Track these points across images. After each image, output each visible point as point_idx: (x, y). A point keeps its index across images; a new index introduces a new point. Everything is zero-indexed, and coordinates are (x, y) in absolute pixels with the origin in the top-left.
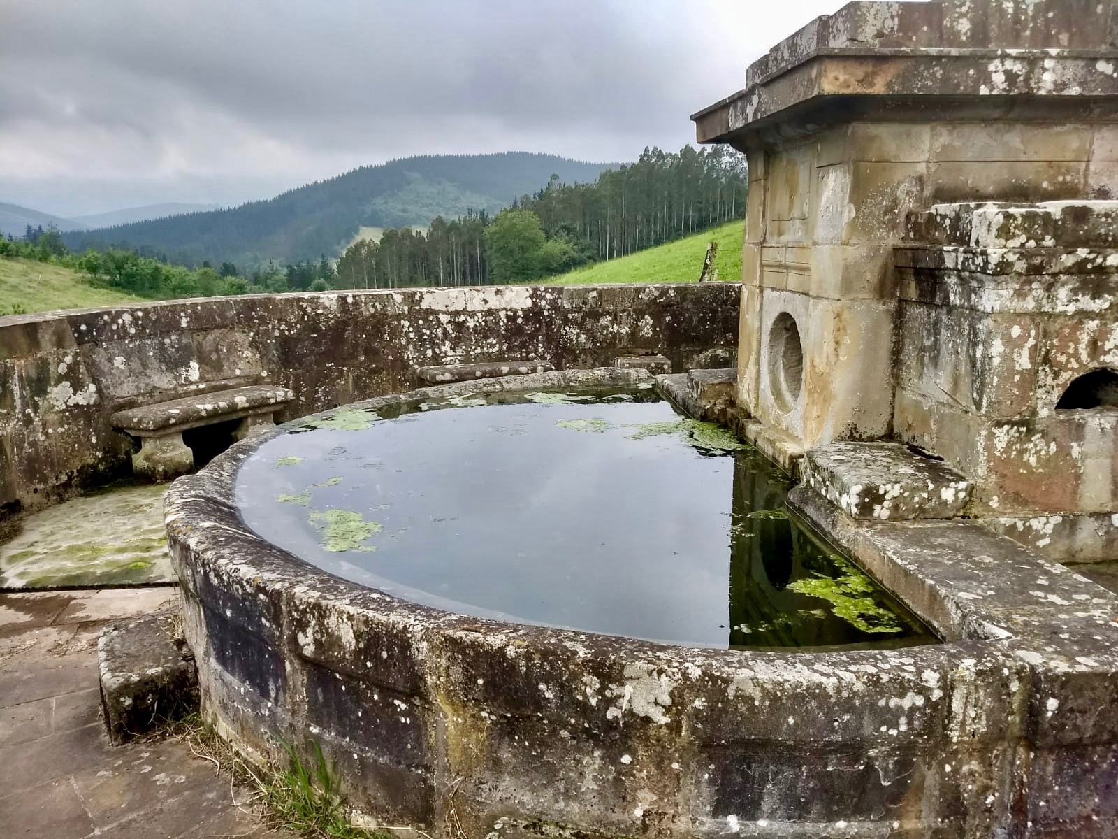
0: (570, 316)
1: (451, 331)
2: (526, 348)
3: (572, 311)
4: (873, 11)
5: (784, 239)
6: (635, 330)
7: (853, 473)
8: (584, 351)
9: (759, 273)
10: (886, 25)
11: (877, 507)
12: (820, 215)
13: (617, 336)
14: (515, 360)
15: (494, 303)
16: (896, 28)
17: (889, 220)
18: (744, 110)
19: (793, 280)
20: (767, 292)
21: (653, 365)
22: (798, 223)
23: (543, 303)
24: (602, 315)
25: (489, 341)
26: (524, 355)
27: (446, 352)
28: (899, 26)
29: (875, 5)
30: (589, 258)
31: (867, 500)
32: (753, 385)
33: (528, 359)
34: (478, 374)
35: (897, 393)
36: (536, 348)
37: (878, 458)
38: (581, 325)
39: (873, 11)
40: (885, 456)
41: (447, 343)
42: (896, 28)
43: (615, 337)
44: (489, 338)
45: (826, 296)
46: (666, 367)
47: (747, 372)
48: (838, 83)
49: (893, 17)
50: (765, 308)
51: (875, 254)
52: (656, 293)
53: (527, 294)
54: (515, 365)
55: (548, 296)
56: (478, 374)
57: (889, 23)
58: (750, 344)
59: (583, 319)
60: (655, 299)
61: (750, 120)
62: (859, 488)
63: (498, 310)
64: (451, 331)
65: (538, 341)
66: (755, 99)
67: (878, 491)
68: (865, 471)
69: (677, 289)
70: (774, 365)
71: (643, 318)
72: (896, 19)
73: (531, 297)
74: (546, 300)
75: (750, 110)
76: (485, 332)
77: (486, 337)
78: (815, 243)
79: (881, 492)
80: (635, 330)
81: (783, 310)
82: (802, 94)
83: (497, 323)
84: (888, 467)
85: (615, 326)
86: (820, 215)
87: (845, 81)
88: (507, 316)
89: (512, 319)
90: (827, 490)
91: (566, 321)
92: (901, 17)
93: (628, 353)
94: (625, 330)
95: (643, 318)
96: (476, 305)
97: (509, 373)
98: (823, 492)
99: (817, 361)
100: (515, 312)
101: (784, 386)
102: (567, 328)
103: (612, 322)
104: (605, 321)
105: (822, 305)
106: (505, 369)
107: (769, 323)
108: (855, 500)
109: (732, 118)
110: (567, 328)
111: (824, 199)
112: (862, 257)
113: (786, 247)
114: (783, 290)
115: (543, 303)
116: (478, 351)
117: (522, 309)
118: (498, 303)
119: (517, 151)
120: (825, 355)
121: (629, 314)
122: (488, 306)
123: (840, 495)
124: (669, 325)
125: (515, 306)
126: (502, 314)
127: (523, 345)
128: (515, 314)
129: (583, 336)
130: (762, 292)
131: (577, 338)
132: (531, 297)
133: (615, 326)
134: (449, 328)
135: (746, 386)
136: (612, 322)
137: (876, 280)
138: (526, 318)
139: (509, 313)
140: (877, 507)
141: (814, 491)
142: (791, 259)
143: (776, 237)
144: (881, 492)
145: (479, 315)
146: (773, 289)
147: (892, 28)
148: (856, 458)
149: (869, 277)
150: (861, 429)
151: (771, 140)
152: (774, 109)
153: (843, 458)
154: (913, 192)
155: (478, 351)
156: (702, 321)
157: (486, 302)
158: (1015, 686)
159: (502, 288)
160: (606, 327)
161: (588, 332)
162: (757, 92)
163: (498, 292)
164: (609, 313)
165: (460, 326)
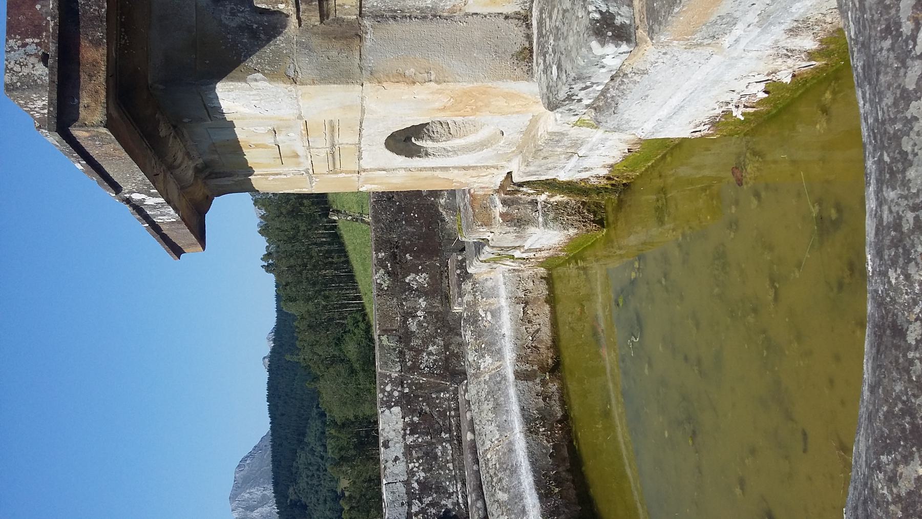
0: (409, 364)
1: (430, 498)
2: (445, 411)
3: (403, 362)
4: (17, 68)
5: (301, 151)
6: (421, 292)
7: (573, 54)
8: (446, 347)
9: (343, 175)
10: (34, 52)
11: (618, 20)
12: (266, 113)
13: (428, 312)
14: (458, 426)
15: (397, 449)
16: (37, 41)
17: (265, 34)
18: (154, 207)
19: (346, 139)
20: (364, 164)
21: (458, 271)
22: (279, 138)
23: (396, 394)
24: (407, 328)
25: (439, 454)
26: (453, 413)
27: (453, 504)
28: (34, 37)
29: (10, 66)
30: (364, 320)
31: (610, 34)
32: (474, 173)
33: (457, 409)
34: (475, 467)
35: (472, 11)
36: (445, 400)
37: (553, 25)
38: (419, 352)
39: (17, 68)
40: (551, 17)
41: (443, 502)
42: (37, 41)
43: (430, 313)
44: (436, 453)
45: (359, 100)
46: (460, 258)
47: (458, 179)
48: (93, 104)
49: (24, 45)
50: (382, 166)
51: (306, 48)
52: (382, 271)
53: (387, 412)
54: (465, 426)
55: (388, 388)
56: (475, 467)
57: (32, 49)
58: (426, 178)
59: (411, 349)
60: (388, 273)
61: (161, 200)
62: (594, 44)
63: (406, 445)
64: (430, 498)
65: (437, 398)
66: (136, 196)
67: (597, 21)
68: (571, 40)
69: (378, 250)
70: (448, 151)
71: (409, 284)
72: (27, 40)
73: (390, 407)
74: (392, 391)
75: (150, 201)
76: (429, 457)
77: (436, 457)
78: (300, 117)
79: (597, 16)
80: (421, 292)
81: (383, 146)
82: (112, 145)
83: (419, 446)
84: (565, 11)
85: (419, 313)
86: (266, 113)
87: (91, 96)
88: (412, 433)
89: (413, 429)
90: (598, 84)
91: (415, 368)
92: (24, 35)
93: (446, 299)
94: (422, 303)
95: (409, 284)
96: (400, 468)
97: (473, 432)
98: (601, 88)
99: (437, 105)
100: (406, 425)
101: (471, 139)
102: (422, 366)
103: (415, 317)
104: (413, 326)
105: (370, 104)
106: (469, 436)
107: (400, 161)
108: (610, 48)
109: (166, 219)
110: (422, 366)
111: (247, 110)
112: (310, 62)
113: (309, 147)
114: (360, 148)
115: (396, 394)
116: (450, 465)
117: (403, 418)
118: (397, 445)
119: (266, 393)
120: (430, 97)
121: (405, 299)
122: (400, 456)
123: (603, 67)
124: (416, 256)
125: (400, 425)
126: (410, 440)
127: (442, 414)
128: (409, 425)
129: (431, 348)
130: (364, 170)
131: (433, 355)
132: (390, 407)
133: (419, 313)
134: (427, 500)
135: (474, 179)
136: (415, 317)
137: (338, 45)
138: (413, 412)
139: (408, 432)
140: (618, 20)
141: (597, 99)
142: (321, 145)
143: (301, 160)
144: (597, 16)
145: (411, 466)
146: (360, 158)
147: (37, 44)
148: (554, 52)
149: (334, 53)
150: (517, 48)
151: (190, 173)
152: (140, 176)
153: (555, 68)
154: (232, 9)
155: (450, 465)
156: (410, 222)
157: (396, 459)
158: (270, 261)
159: (381, 440)
160: (420, 324)
161: (426, 344)
162: (127, 195)
163: (386, 445)
164: (405, 321)
165: (425, 487)
